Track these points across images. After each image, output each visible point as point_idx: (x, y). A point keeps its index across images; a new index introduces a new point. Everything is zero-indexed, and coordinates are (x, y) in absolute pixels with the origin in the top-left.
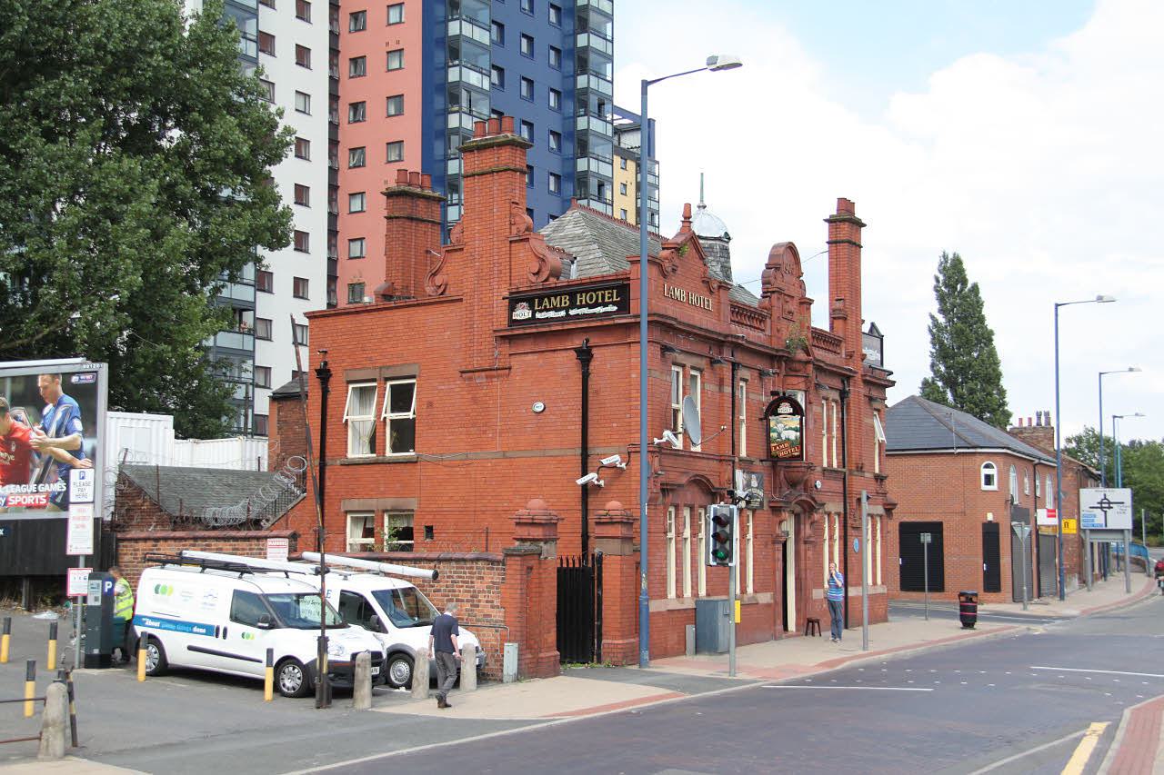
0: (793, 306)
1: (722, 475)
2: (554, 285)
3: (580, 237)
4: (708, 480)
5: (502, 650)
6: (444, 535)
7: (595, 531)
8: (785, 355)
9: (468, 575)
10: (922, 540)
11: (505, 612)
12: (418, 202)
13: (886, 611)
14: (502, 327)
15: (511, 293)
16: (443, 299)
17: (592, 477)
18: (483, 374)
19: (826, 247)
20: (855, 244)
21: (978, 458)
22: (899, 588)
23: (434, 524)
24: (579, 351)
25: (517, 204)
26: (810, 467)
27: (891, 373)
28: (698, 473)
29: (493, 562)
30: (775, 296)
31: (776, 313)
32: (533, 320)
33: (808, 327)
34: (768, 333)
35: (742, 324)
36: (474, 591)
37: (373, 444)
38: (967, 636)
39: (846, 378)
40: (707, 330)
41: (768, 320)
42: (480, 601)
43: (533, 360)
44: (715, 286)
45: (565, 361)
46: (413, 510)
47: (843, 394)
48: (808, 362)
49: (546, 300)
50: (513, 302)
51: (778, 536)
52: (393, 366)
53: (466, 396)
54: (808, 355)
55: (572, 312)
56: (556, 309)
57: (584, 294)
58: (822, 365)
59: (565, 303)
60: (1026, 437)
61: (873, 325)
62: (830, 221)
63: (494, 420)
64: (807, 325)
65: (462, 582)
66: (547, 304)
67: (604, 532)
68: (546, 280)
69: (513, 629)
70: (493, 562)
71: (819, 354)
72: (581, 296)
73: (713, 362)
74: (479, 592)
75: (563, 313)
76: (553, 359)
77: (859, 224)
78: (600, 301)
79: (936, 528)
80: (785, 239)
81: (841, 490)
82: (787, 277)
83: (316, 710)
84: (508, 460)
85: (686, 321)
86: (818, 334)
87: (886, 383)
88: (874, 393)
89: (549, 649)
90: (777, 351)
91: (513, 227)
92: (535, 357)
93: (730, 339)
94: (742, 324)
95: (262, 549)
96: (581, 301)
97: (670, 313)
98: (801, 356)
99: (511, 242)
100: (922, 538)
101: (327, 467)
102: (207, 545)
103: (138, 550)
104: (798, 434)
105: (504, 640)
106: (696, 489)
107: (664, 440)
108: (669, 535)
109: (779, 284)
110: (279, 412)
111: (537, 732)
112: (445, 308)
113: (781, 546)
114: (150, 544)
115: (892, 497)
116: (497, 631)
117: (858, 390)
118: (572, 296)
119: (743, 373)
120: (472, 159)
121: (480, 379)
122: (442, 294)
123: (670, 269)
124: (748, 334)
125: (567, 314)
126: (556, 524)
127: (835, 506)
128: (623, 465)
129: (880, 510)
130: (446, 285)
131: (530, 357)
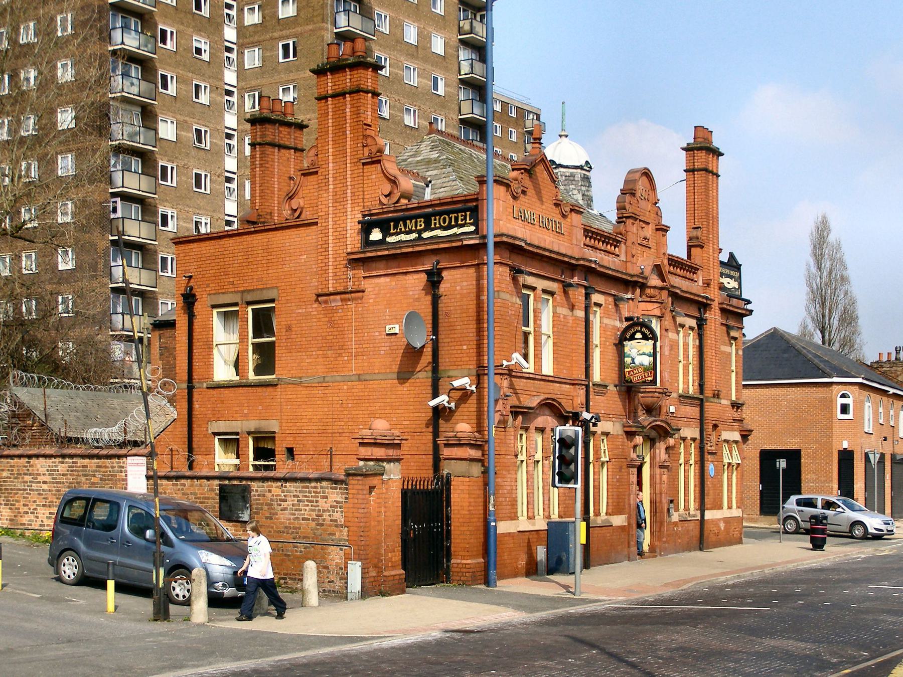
0: (649, 231)
1: (575, 399)
2: (404, 207)
3: (436, 161)
4: (560, 404)
5: (346, 567)
6: (303, 456)
7: (446, 452)
8: (640, 280)
9: (313, 494)
10: (778, 466)
11: (348, 531)
12: (281, 129)
13: (741, 534)
14: (356, 250)
15: (364, 216)
16: (298, 222)
17: (443, 399)
18: (338, 297)
19: (684, 175)
20: (712, 172)
21: (835, 388)
22: (758, 513)
23: (294, 446)
24: (429, 273)
25: (370, 126)
26: (665, 393)
27: (749, 302)
28: (550, 396)
29: (336, 482)
30: (629, 221)
31: (631, 238)
32: (382, 242)
33: (664, 254)
34: (623, 258)
35: (596, 248)
36: (319, 510)
37: (238, 366)
38: (814, 558)
39: (703, 306)
40: (558, 253)
41: (623, 245)
42: (324, 520)
43: (386, 282)
44: (568, 209)
45: (416, 282)
46: (274, 432)
47: (701, 323)
48: (662, 289)
49: (401, 223)
50: (366, 227)
51: (632, 460)
52: (253, 290)
53: (322, 320)
54: (663, 280)
55: (426, 235)
56: (410, 232)
57: (437, 218)
58: (678, 291)
59: (421, 226)
60: (886, 371)
61: (732, 255)
62: (688, 149)
63: (349, 343)
64: (663, 251)
65: (308, 501)
66: (402, 227)
67: (454, 454)
68: (397, 202)
69: (356, 548)
70: (336, 482)
71: (676, 281)
72: (435, 219)
73: (566, 286)
74: (324, 511)
75: (414, 236)
76: (405, 282)
77: (717, 153)
78: (453, 223)
79: (794, 456)
80: (640, 165)
81: (698, 416)
82: (643, 204)
83: (362, 602)
84: (364, 383)
85: (536, 243)
86: (674, 262)
87: (744, 312)
88: (732, 323)
89: (394, 567)
90: (632, 276)
91: (365, 148)
92: (387, 279)
93: (582, 262)
94: (596, 248)
95: (123, 467)
96: (435, 224)
97: (519, 235)
98: (655, 281)
99: (364, 164)
100: (778, 463)
101: (195, 390)
102: (73, 463)
103: (14, 466)
104: (652, 359)
105: (347, 558)
106: (547, 411)
107: (513, 362)
108: (520, 458)
109: (630, 209)
110: (160, 339)
111: (357, 656)
112: (302, 230)
113: (636, 470)
114: (24, 461)
115: (748, 424)
116: (341, 549)
117: (714, 317)
118: (427, 218)
119: (596, 298)
120: (326, 82)
121: (336, 301)
122: (298, 217)
123: (519, 191)
124: (602, 259)
125: (420, 238)
126: (399, 445)
127: (690, 432)
128: (473, 388)
129: (736, 436)
130: (302, 208)
131: (383, 280)
